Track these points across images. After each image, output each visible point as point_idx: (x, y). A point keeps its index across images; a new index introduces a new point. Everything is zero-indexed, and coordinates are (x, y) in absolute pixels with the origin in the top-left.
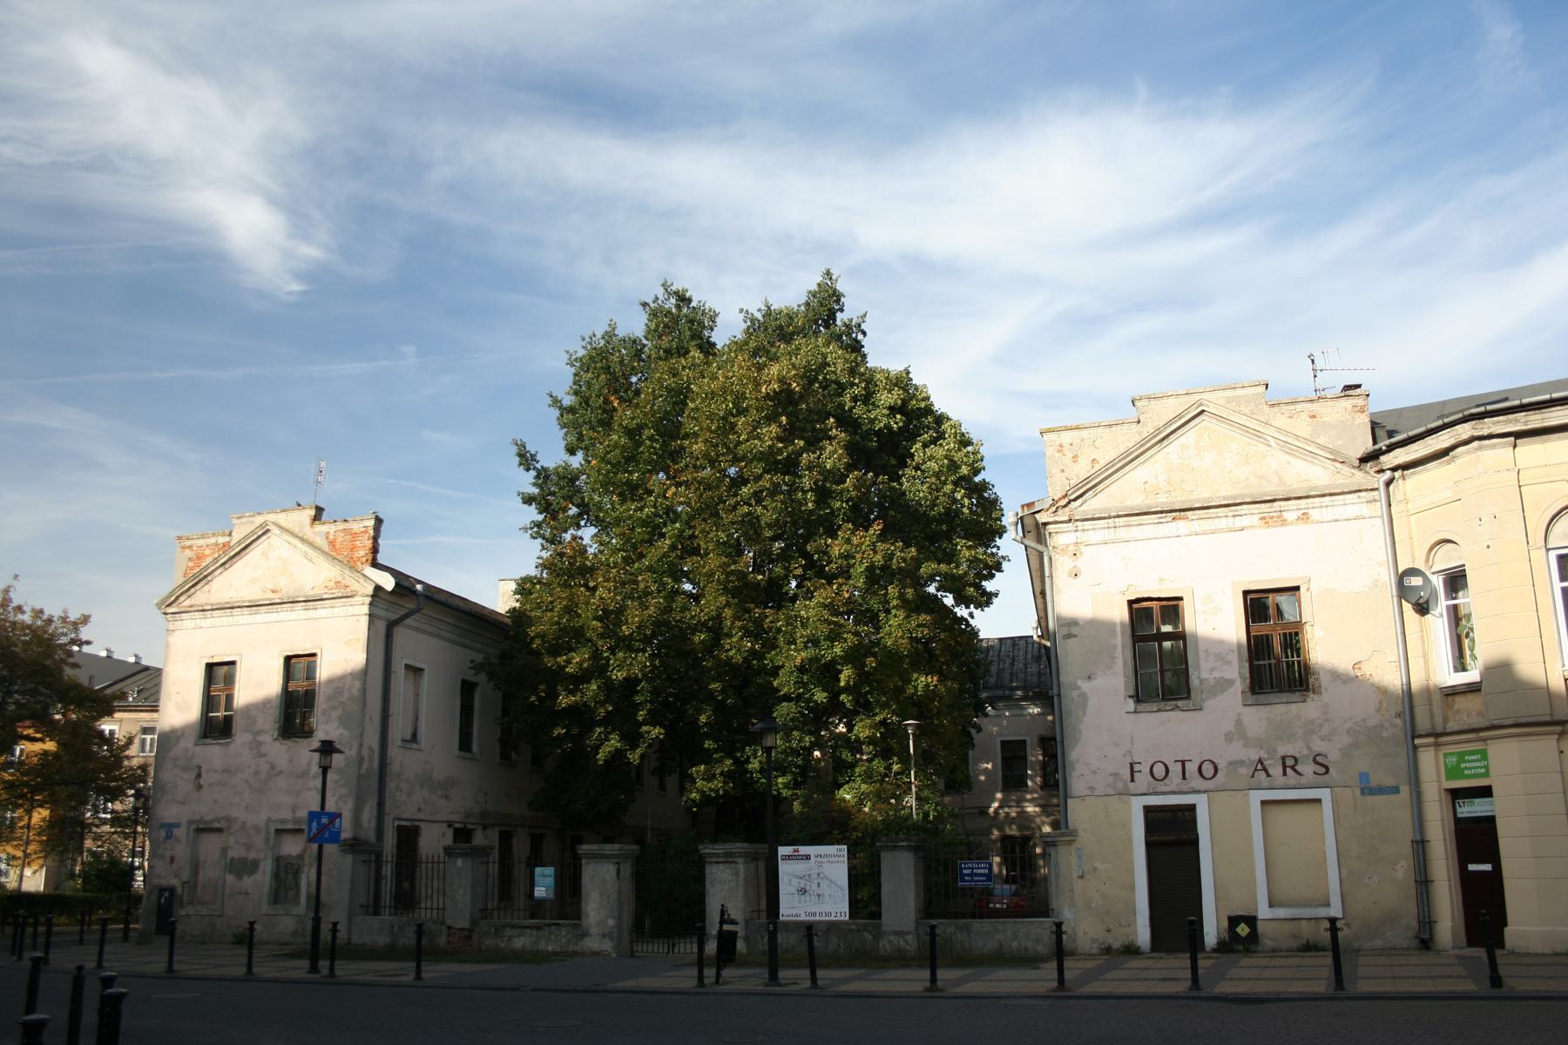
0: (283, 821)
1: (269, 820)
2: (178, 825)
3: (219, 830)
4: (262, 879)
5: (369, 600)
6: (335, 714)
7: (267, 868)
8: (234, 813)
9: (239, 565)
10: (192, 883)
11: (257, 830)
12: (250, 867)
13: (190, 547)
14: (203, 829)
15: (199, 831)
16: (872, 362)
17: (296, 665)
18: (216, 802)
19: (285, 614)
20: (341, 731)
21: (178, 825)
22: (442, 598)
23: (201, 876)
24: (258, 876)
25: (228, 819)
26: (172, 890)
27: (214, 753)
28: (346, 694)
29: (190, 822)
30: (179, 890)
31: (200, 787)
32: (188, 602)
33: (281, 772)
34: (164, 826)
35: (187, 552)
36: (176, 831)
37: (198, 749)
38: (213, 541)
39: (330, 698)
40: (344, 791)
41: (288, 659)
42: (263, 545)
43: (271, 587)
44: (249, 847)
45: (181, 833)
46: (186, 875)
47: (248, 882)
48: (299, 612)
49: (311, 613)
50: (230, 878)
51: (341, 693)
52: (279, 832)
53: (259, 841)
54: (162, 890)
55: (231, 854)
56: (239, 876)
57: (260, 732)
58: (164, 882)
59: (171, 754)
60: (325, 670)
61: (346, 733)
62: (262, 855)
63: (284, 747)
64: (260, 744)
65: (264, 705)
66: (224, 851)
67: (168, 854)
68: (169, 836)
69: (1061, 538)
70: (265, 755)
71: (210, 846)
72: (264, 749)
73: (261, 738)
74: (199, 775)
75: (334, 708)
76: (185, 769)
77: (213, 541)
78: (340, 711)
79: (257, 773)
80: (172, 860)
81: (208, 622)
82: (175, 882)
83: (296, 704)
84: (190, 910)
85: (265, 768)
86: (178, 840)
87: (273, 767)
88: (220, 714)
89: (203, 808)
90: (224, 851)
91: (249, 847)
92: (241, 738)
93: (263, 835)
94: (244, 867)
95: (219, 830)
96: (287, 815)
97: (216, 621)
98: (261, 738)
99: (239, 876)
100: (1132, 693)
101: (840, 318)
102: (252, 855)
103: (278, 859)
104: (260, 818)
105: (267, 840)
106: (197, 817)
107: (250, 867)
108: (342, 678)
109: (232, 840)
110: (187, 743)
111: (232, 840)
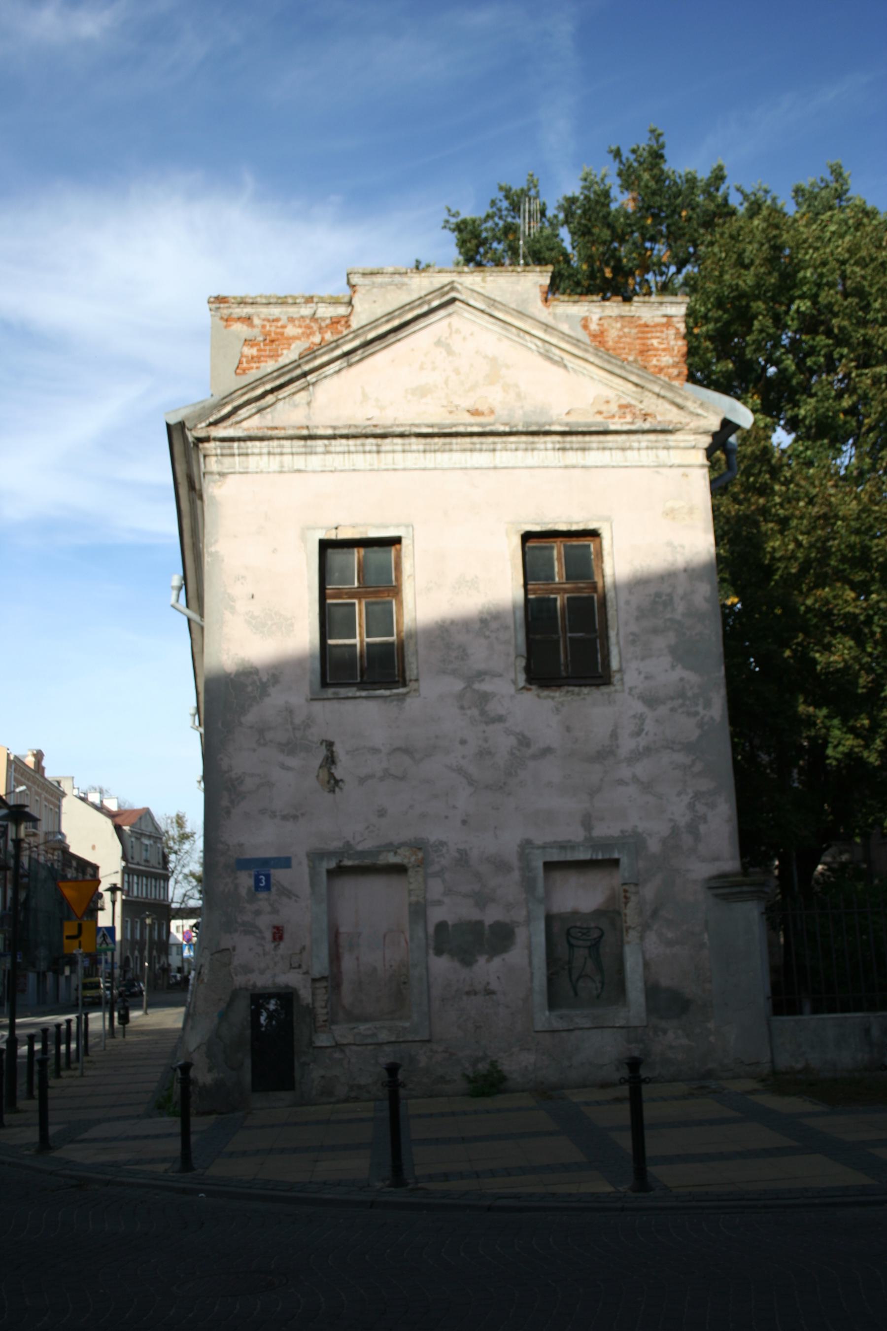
0: (563, 846)
1: (526, 845)
2: (285, 862)
3: (400, 870)
5: (707, 441)
6: (660, 643)
7: (532, 940)
8: (433, 834)
9: (381, 360)
10: (333, 981)
11: (501, 866)
12: (501, 937)
13: (248, 320)
14: (347, 867)
15: (339, 872)
16: (666, 167)
17: (558, 556)
18: (382, 813)
19: (508, 455)
20: (680, 672)
21: (285, 862)
23: (348, 963)
24: (515, 956)
25: (418, 846)
26: (287, 997)
27: (363, 718)
28: (680, 608)
29: (316, 856)
30: (305, 995)
31: (334, 784)
32: (255, 421)
33: (547, 751)
34: (244, 864)
36: (279, 875)
37: (317, 706)
38: (306, 311)
39: (642, 614)
40: (705, 784)
41: (325, 545)
42: (437, 327)
44: (482, 900)
45: (297, 877)
46: (320, 966)
47: (488, 969)
48: (546, 453)
49: (572, 457)
50: (442, 966)
51: (668, 602)
52: (549, 866)
53: (509, 887)
54: (258, 999)
55: (436, 915)
56: (467, 960)
57: (481, 675)
58: (262, 981)
59: (250, 718)
60: (622, 560)
61: (692, 677)
62: (520, 915)
63: (549, 704)
64: (485, 697)
65: (486, 623)
66: (418, 911)
67: (265, 922)
68: (263, 884)
69: (213, 461)
70: (500, 719)
71: (371, 905)
72: (494, 708)
74: (330, 760)
75: (655, 631)
76: (290, 748)
77: (306, 311)
78: (671, 638)
79: (484, 753)
80: (278, 934)
81: (315, 462)
82: (292, 979)
83: (564, 617)
84: (342, 1032)
85: (504, 744)
87: (524, 741)
88: (359, 640)
89: (350, 823)
90: (418, 911)
91: (482, 900)
92: (431, 689)
93: (516, 875)
96: (577, 834)
97: (336, 461)
98: (486, 686)
99: (467, 960)
102: (492, 915)
103: (549, 919)
104: (507, 843)
105: (528, 884)
106: (335, 845)
107: (501, 937)
108: (668, 577)
109: (436, 888)
110: (297, 696)
111: (436, 888)
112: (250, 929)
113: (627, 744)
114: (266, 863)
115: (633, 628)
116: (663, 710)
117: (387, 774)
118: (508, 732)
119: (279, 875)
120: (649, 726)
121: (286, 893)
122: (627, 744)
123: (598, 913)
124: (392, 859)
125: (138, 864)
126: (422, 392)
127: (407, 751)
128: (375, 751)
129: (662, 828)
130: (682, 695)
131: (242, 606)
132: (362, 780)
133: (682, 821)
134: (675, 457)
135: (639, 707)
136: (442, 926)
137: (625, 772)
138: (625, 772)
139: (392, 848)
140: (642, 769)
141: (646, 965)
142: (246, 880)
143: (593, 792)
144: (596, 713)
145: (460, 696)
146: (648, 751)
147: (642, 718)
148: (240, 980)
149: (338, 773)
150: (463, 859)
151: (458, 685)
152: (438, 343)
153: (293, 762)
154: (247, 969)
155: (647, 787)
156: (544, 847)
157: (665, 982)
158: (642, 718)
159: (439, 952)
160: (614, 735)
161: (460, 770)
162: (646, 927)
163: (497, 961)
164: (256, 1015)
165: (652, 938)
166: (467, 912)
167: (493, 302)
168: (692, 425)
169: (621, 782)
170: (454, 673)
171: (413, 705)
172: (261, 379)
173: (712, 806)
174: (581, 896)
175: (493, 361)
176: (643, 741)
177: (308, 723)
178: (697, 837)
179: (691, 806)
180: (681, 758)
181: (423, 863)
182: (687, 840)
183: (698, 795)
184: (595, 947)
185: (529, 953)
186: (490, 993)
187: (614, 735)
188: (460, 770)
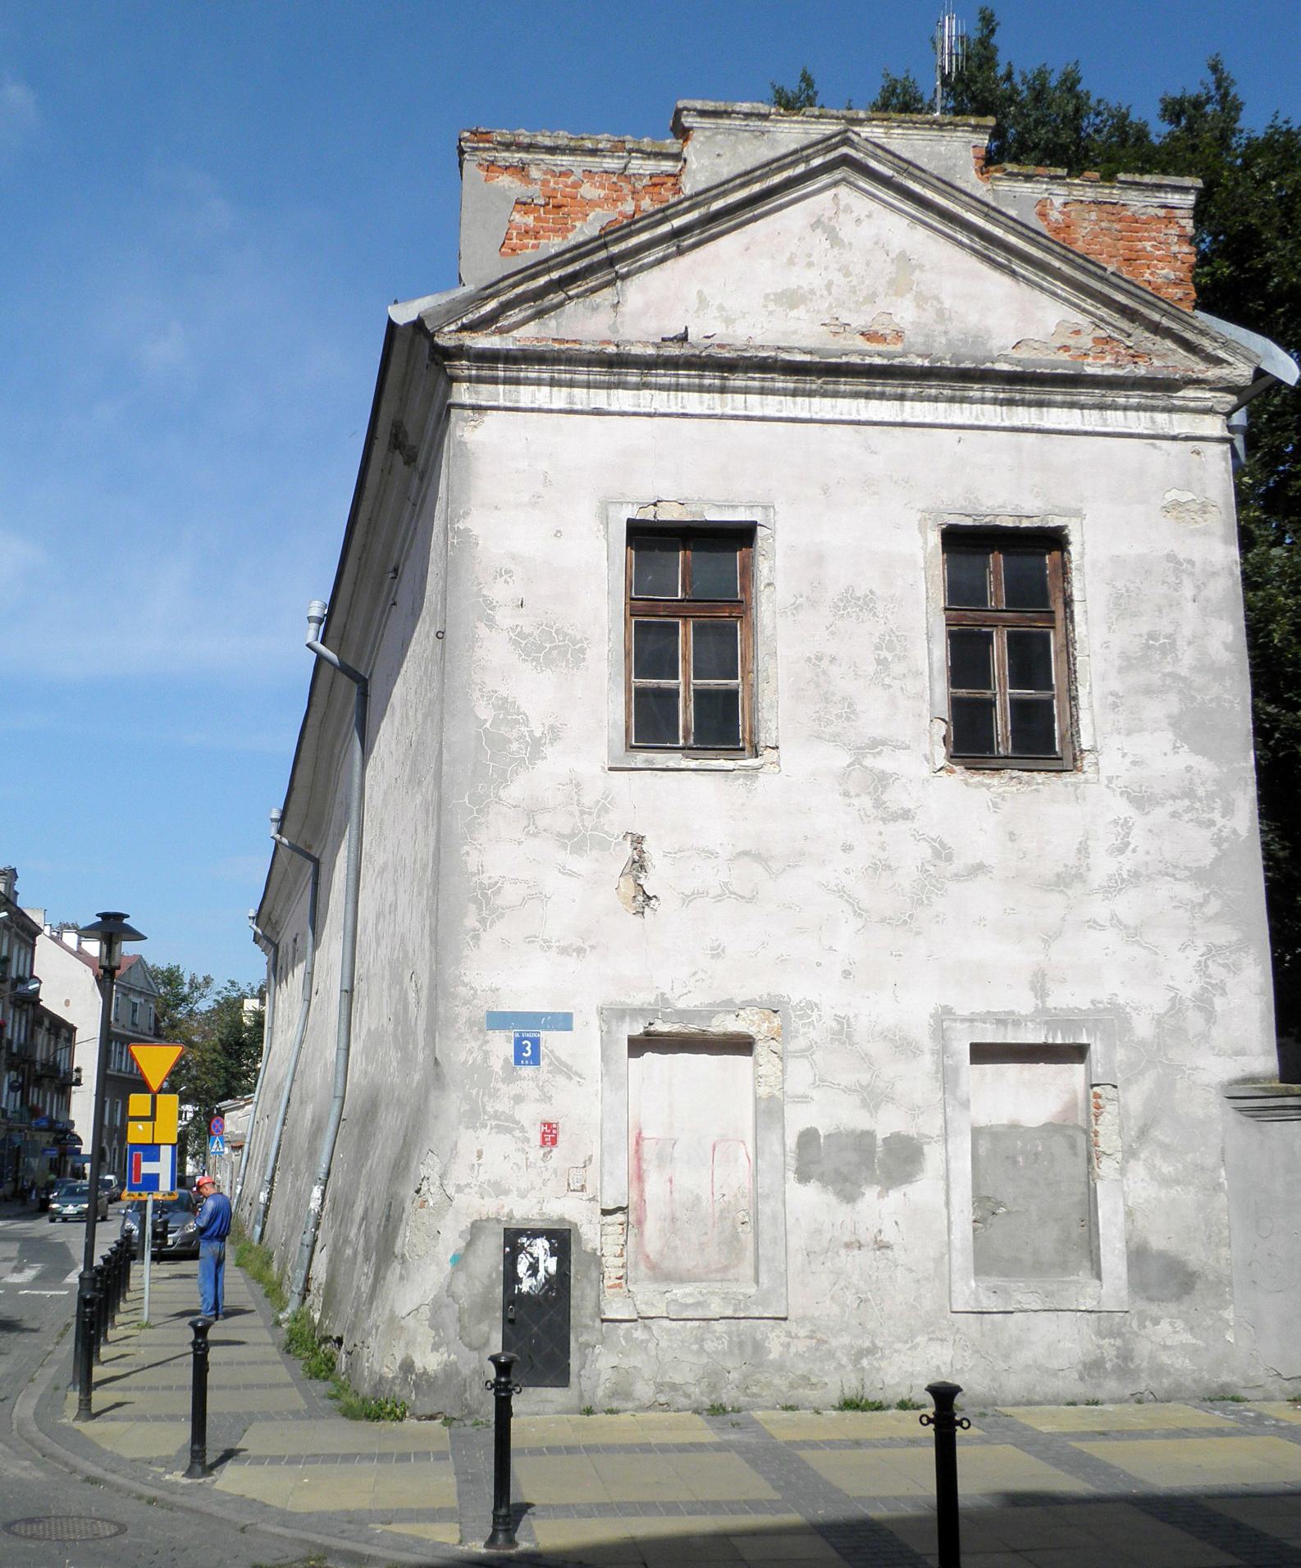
1: (943, 1017)
2: (563, 1022)
3: (741, 1045)
4: (931, 1209)
8: (796, 990)
22: (710, 530)
24: (924, 1189)
29: (612, 1014)
33: (979, 869)
34: (498, 1020)
35: (505, 180)
36: (550, 1040)
43: (859, 321)
44: (872, 1098)
47: (879, 1208)
50: (808, 1201)
51: (1170, 648)
59: (514, 791)
64: (882, 780)
73: (883, 762)
74: (639, 865)
76: (576, 842)
79: (880, 868)
80: (550, 1135)
85: (911, 855)
86: (563, 1069)
87: (943, 853)
90: (769, 1112)
91: (872, 1098)
93: (927, 1062)
94: (859, 1162)
95: (741, 1045)
98: (883, 762)
100: (396, 1268)
101: (1079, 88)
102: (887, 1124)
106: (641, 998)
111: (800, 1075)
133: (1188, 991)
134: (1181, 424)
140: (1128, 905)
150: (843, 1032)
155: (1133, 933)
169: (1093, 924)
173: (1235, 969)
176: (1127, 862)
180: (1189, 891)
183: (1212, 951)
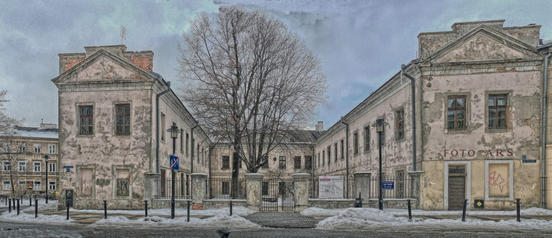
8: (97, 163)
20: (143, 133)
21: (72, 167)
25: (95, 165)
29: (77, 166)
30: (75, 191)
33: (117, 148)
34: (65, 167)
36: (71, 169)
37: (78, 139)
47: (105, 188)
50: (97, 187)
54: (67, 191)
55: (97, 178)
57: (106, 133)
58: (68, 188)
59: (66, 140)
62: (111, 178)
63: (118, 139)
64: (107, 137)
66: (94, 177)
67: (68, 177)
68: (68, 171)
70: (109, 141)
72: (108, 139)
74: (80, 148)
75: (139, 124)
77: (76, 56)
79: (106, 148)
82: (73, 188)
85: (110, 146)
87: (113, 146)
93: (111, 171)
98: (107, 135)
102: (107, 178)
103: (118, 180)
107: (108, 182)
112: (66, 179)
113: (132, 147)
114: (69, 167)
115: (135, 124)
116: (139, 140)
117: (89, 152)
118: (110, 144)
119: (71, 169)
120: (136, 143)
121: (72, 172)
122: (132, 147)
123: (127, 179)
124: (90, 167)
125: (391, 197)
126: (98, 74)
127: (93, 147)
128: (87, 147)
129: (137, 163)
130: (143, 137)
131: (65, 119)
132: (85, 152)
133: (141, 162)
135: (134, 140)
136: (98, 180)
137: (131, 152)
138: (131, 152)
139: (90, 165)
140: (134, 152)
141: (133, 189)
142: (65, 170)
143: (125, 156)
144: (127, 141)
145: (102, 137)
146: (135, 148)
147: (135, 142)
148: (64, 188)
149: (81, 151)
151: (102, 135)
152: (101, 63)
153: (73, 149)
154: (65, 186)
155: (135, 155)
156: (116, 166)
157: (136, 192)
158: (135, 142)
159: (97, 184)
160: (129, 145)
161: (102, 151)
162: (133, 181)
163: (107, 187)
164: (66, 194)
165: (134, 184)
166: (102, 177)
167: (110, 54)
168: (148, 80)
170: (102, 132)
171: (94, 139)
172: (393, 77)
174: (124, 176)
175: (112, 67)
176: (135, 146)
177: (76, 141)
178: (143, 165)
179: (143, 159)
180: (141, 150)
181: (95, 168)
182: (141, 166)
184: (126, 185)
185: (113, 185)
186: (105, 192)
187: (129, 145)
188: (102, 151)
